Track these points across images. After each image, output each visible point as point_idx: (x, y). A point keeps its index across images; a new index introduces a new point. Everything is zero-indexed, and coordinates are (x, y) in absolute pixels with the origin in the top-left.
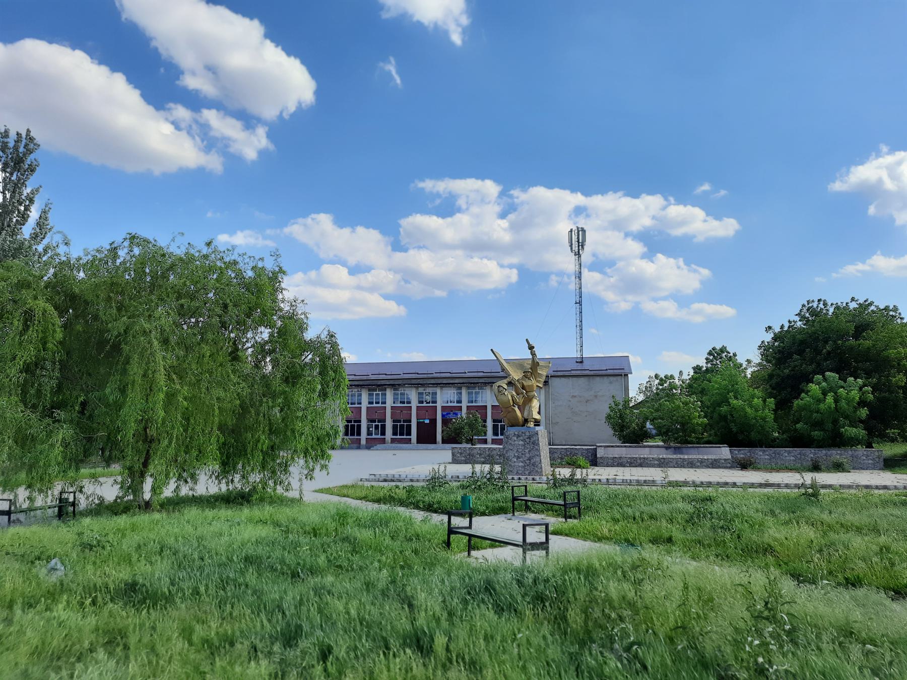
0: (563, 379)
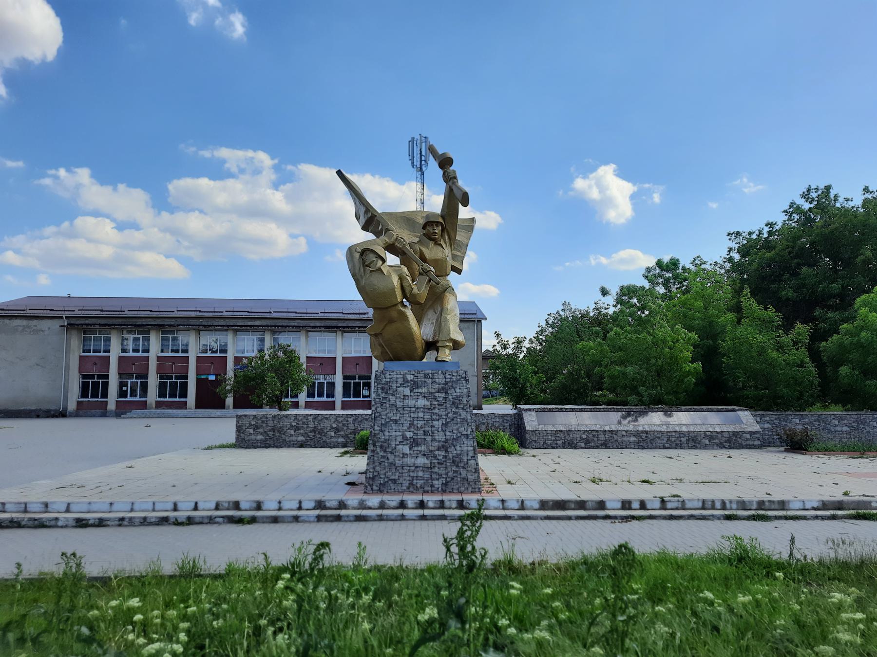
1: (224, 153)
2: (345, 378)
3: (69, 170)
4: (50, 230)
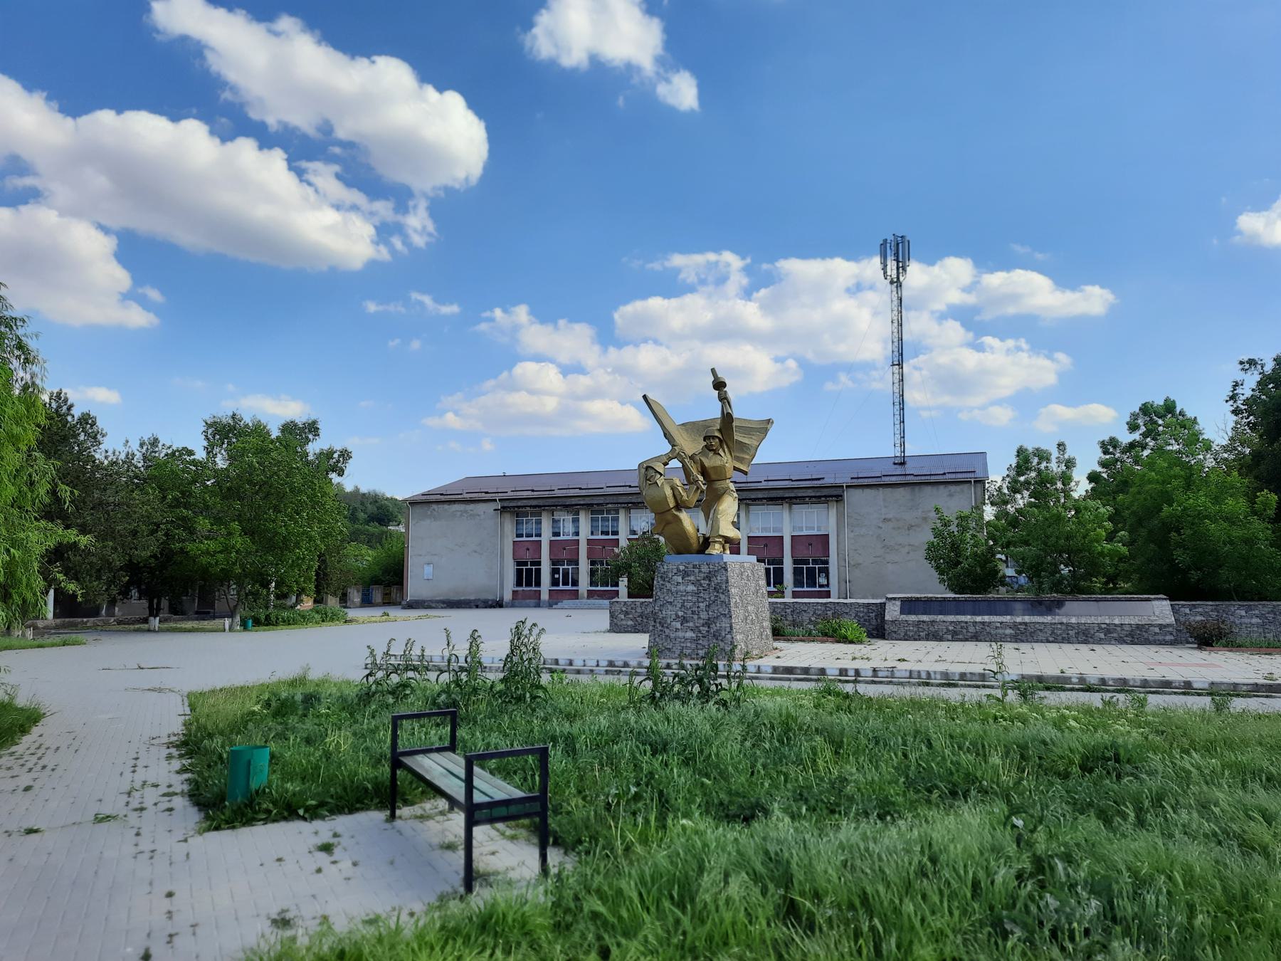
0: (868, 491)
1: (678, 260)
2: (795, 562)
3: (505, 311)
4: (491, 383)
